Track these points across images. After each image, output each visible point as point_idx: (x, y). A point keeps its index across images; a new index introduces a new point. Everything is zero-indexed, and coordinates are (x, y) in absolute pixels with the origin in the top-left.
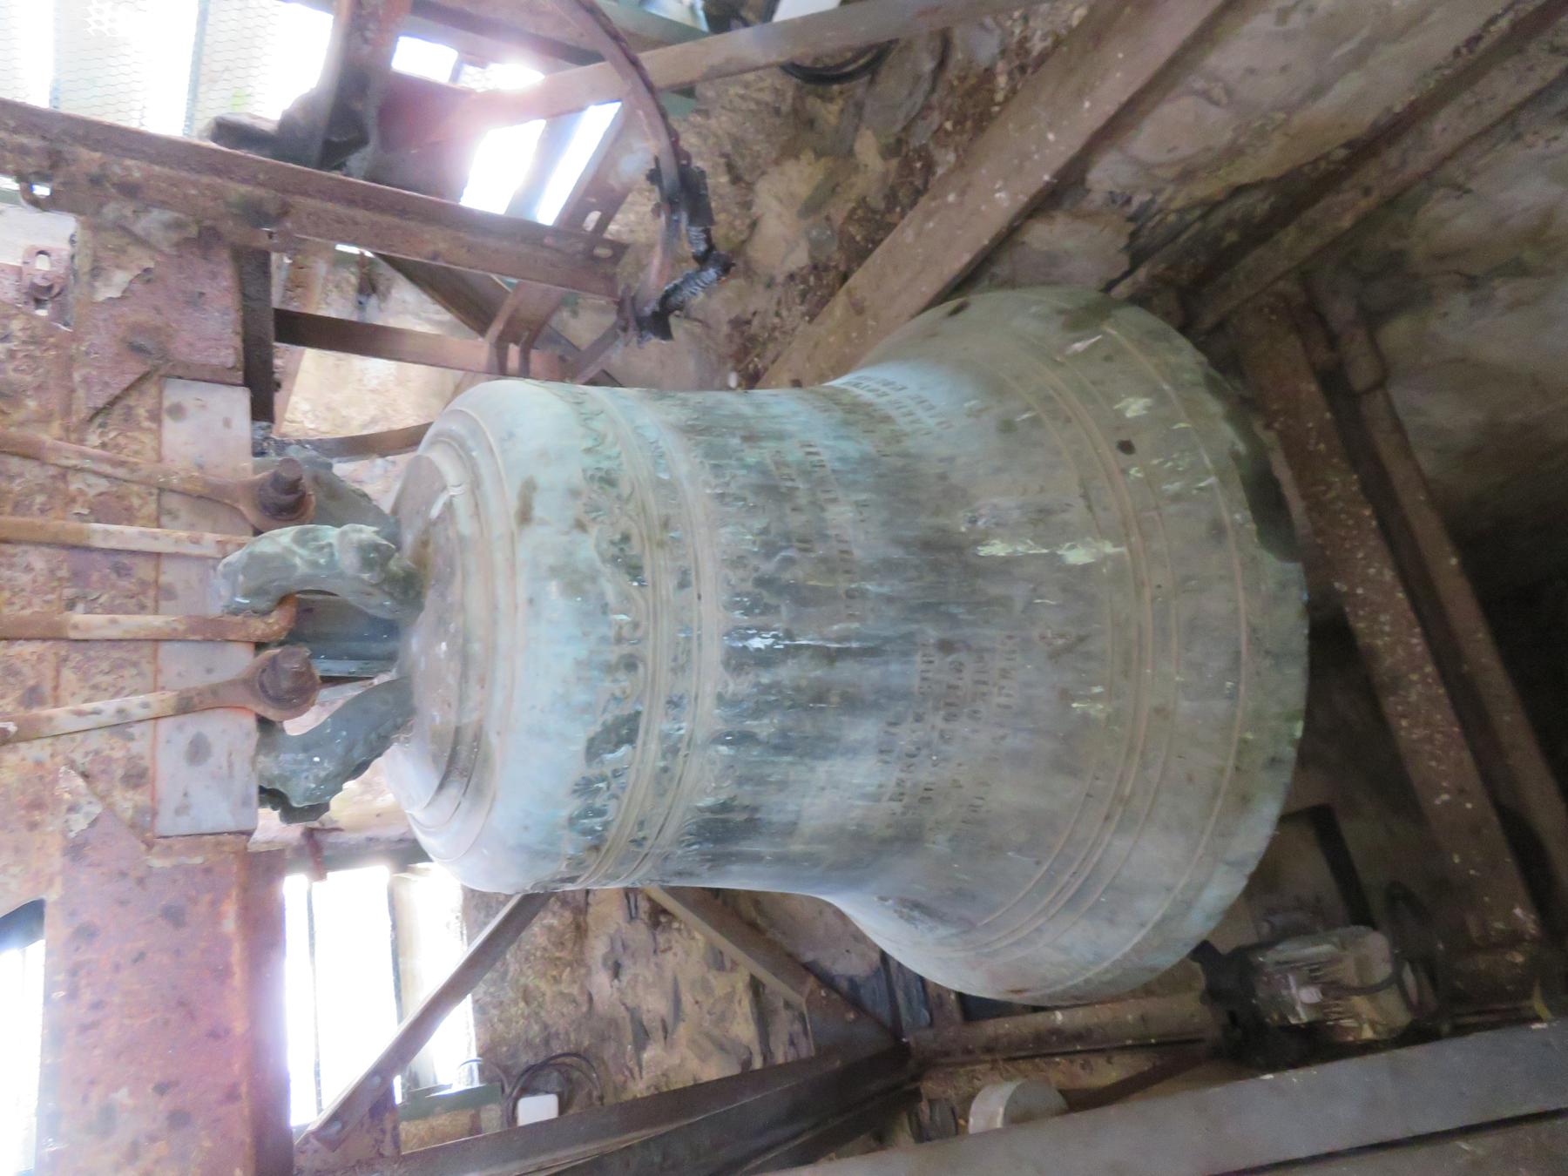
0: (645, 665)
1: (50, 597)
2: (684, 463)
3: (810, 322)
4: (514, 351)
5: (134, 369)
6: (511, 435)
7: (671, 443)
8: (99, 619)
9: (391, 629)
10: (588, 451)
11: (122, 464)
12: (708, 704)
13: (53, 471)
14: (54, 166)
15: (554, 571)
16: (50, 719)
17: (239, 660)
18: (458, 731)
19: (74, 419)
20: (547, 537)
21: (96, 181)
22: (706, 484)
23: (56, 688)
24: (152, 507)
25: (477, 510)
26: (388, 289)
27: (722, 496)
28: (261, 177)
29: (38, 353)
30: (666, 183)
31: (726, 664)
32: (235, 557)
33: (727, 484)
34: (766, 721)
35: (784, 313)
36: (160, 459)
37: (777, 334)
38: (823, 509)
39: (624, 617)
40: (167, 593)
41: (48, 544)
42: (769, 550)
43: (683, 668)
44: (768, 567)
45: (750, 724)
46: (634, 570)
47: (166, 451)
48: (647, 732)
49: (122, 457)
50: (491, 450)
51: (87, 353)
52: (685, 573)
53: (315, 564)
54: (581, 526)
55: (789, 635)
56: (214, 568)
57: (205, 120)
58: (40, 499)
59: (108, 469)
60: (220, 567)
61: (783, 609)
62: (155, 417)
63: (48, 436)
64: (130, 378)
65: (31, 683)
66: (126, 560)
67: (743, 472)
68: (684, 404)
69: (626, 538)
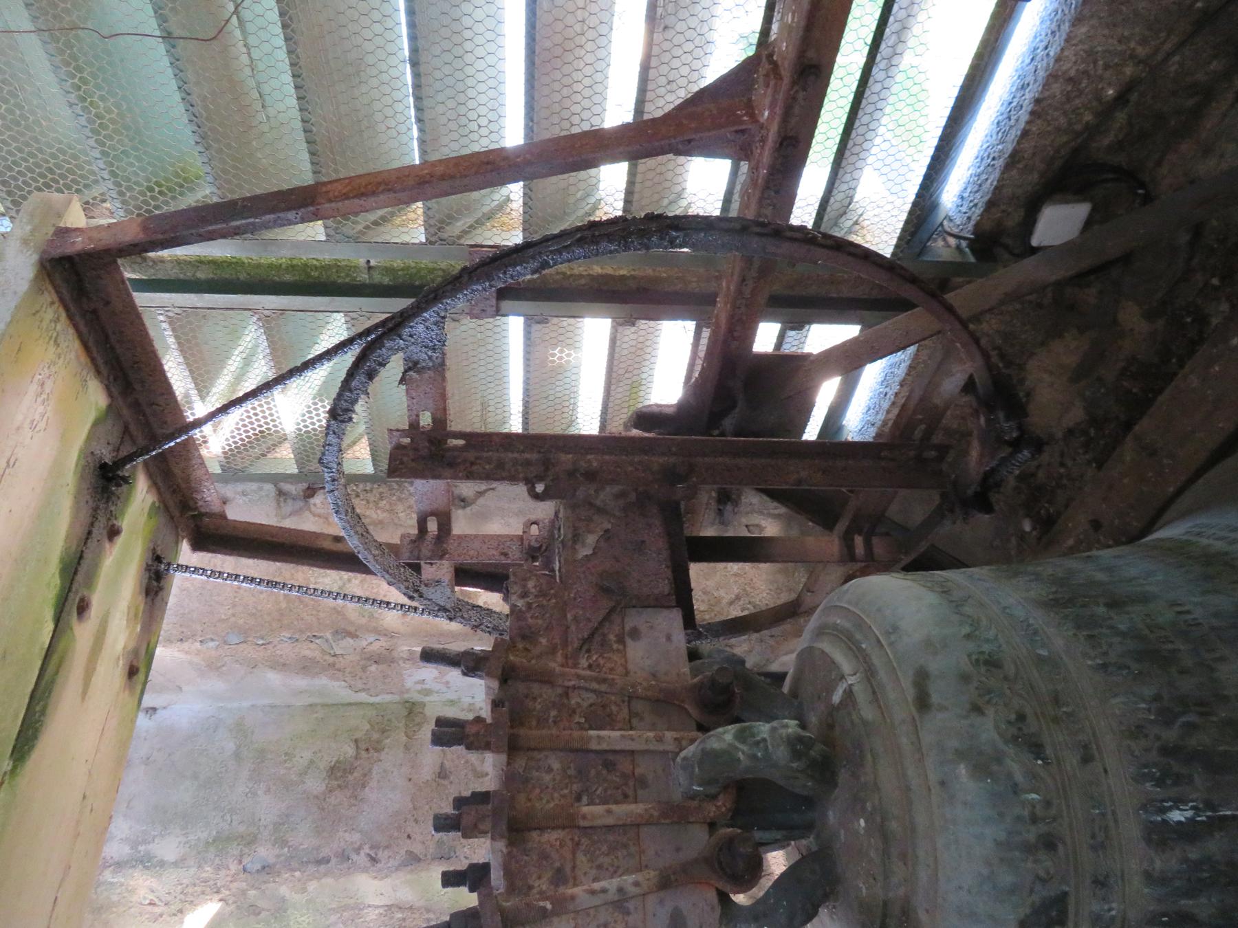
0: (1064, 843)
1: (566, 791)
2: (1058, 638)
3: (1099, 467)
4: (859, 541)
5: (606, 604)
6: (895, 629)
7: (1038, 618)
8: (599, 809)
9: (809, 802)
10: (968, 636)
11: (604, 681)
12: (1137, 882)
13: (559, 691)
14: (547, 469)
15: (961, 755)
16: (573, 898)
17: (697, 840)
18: (885, 904)
19: (570, 649)
20: (946, 721)
21: (571, 474)
22: (1085, 655)
23: (574, 868)
24: (625, 713)
25: (876, 695)
26: (739, 496)
27: (1104, 666)
28: (674, 449)
29: (545, 602)
30: (981, 391)
31: (1149, 841)
32: (690, 751)
33: (1106, 654)
34: (1203, 900)
35: (1070, 463)
36: (627, 673)
37: (1065, 481)
38: (1212, 670)
39: (1034, 796)
40: (642, 782)
41: (561, 750)
42: (1167, 717)
43: (1102, 846)
44: (1171, 735)
45: (1186, 903)
46: (1037, 749)
47: (631, 667)
48: (1076, 914)
49: (602, 675)
50: (879, 641)
51: (575, 599)
52: (1086, 747)
53: (754, 757)
54: (977, 709)
55: (1210, 805)
56: (674, 760)
57: (625, 415)
58: (553, 713)
59: (595, 685)
60: (679, 759)
61: (1198, 780)
62: (621, 640)
63: (554, 665)
64: (603, 612)
65: (557, 864)
66: (611, 757)
67: (1116, 640)
68: (1037, 577)
69: (1021, 717)
